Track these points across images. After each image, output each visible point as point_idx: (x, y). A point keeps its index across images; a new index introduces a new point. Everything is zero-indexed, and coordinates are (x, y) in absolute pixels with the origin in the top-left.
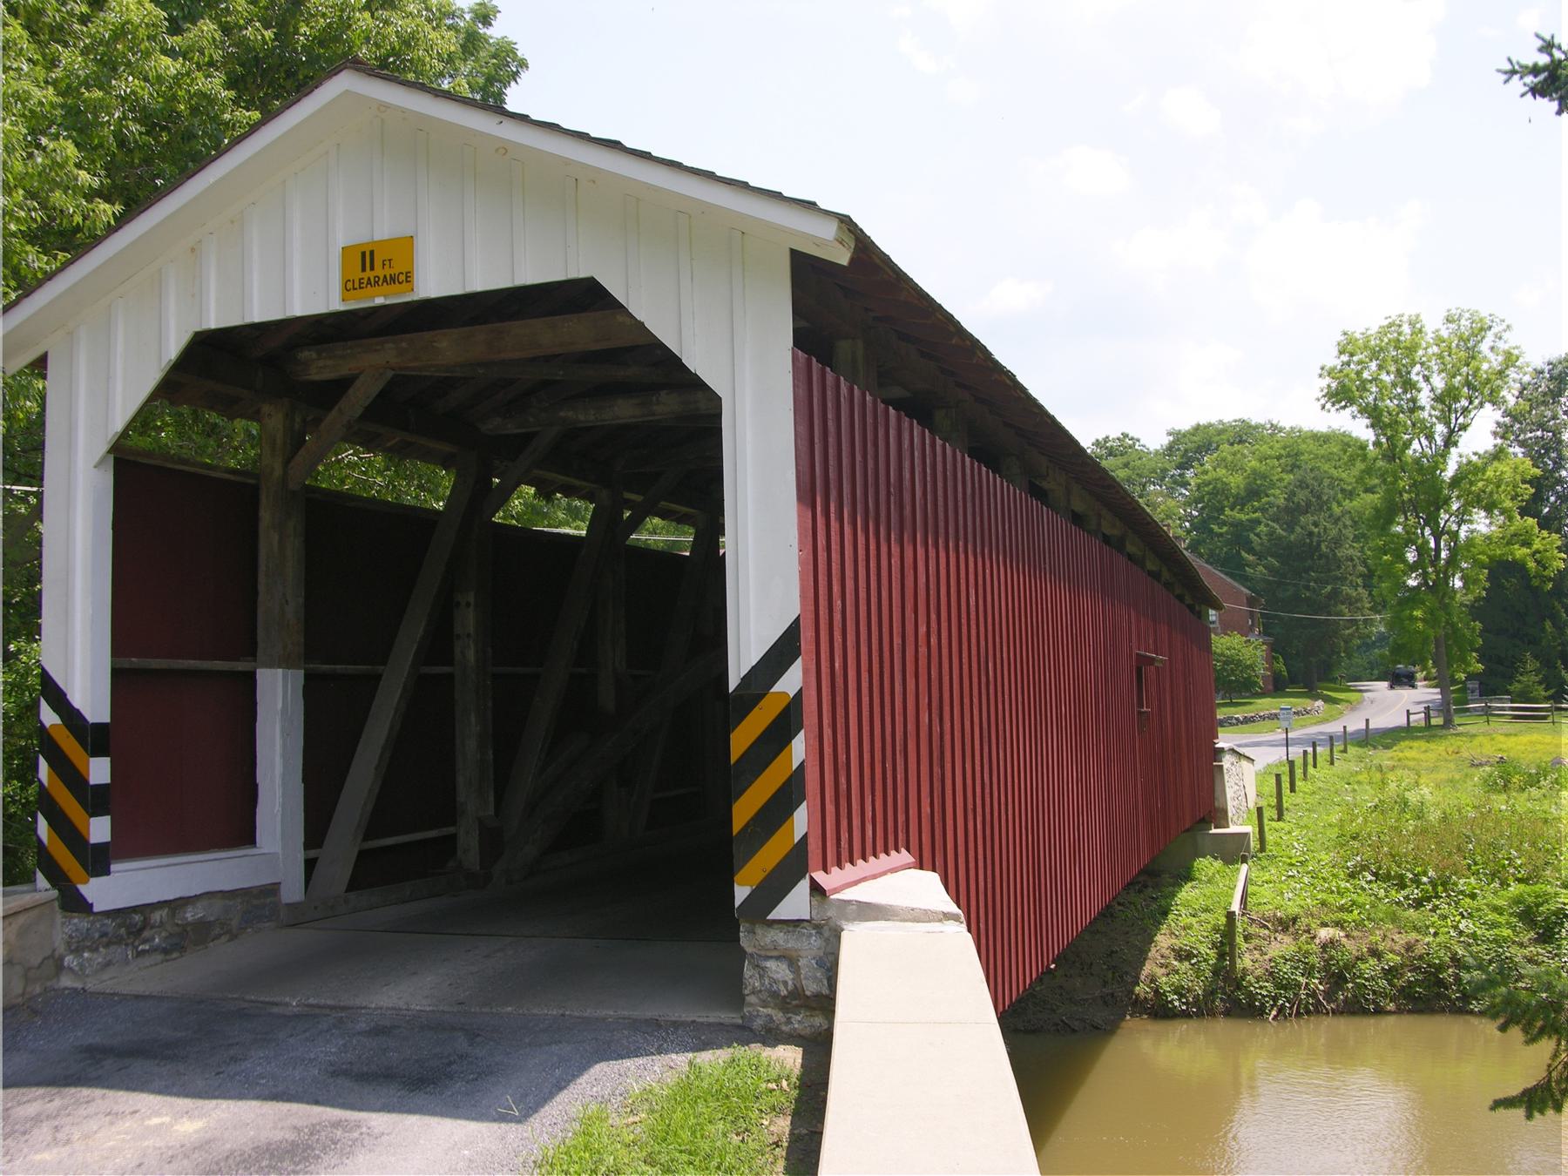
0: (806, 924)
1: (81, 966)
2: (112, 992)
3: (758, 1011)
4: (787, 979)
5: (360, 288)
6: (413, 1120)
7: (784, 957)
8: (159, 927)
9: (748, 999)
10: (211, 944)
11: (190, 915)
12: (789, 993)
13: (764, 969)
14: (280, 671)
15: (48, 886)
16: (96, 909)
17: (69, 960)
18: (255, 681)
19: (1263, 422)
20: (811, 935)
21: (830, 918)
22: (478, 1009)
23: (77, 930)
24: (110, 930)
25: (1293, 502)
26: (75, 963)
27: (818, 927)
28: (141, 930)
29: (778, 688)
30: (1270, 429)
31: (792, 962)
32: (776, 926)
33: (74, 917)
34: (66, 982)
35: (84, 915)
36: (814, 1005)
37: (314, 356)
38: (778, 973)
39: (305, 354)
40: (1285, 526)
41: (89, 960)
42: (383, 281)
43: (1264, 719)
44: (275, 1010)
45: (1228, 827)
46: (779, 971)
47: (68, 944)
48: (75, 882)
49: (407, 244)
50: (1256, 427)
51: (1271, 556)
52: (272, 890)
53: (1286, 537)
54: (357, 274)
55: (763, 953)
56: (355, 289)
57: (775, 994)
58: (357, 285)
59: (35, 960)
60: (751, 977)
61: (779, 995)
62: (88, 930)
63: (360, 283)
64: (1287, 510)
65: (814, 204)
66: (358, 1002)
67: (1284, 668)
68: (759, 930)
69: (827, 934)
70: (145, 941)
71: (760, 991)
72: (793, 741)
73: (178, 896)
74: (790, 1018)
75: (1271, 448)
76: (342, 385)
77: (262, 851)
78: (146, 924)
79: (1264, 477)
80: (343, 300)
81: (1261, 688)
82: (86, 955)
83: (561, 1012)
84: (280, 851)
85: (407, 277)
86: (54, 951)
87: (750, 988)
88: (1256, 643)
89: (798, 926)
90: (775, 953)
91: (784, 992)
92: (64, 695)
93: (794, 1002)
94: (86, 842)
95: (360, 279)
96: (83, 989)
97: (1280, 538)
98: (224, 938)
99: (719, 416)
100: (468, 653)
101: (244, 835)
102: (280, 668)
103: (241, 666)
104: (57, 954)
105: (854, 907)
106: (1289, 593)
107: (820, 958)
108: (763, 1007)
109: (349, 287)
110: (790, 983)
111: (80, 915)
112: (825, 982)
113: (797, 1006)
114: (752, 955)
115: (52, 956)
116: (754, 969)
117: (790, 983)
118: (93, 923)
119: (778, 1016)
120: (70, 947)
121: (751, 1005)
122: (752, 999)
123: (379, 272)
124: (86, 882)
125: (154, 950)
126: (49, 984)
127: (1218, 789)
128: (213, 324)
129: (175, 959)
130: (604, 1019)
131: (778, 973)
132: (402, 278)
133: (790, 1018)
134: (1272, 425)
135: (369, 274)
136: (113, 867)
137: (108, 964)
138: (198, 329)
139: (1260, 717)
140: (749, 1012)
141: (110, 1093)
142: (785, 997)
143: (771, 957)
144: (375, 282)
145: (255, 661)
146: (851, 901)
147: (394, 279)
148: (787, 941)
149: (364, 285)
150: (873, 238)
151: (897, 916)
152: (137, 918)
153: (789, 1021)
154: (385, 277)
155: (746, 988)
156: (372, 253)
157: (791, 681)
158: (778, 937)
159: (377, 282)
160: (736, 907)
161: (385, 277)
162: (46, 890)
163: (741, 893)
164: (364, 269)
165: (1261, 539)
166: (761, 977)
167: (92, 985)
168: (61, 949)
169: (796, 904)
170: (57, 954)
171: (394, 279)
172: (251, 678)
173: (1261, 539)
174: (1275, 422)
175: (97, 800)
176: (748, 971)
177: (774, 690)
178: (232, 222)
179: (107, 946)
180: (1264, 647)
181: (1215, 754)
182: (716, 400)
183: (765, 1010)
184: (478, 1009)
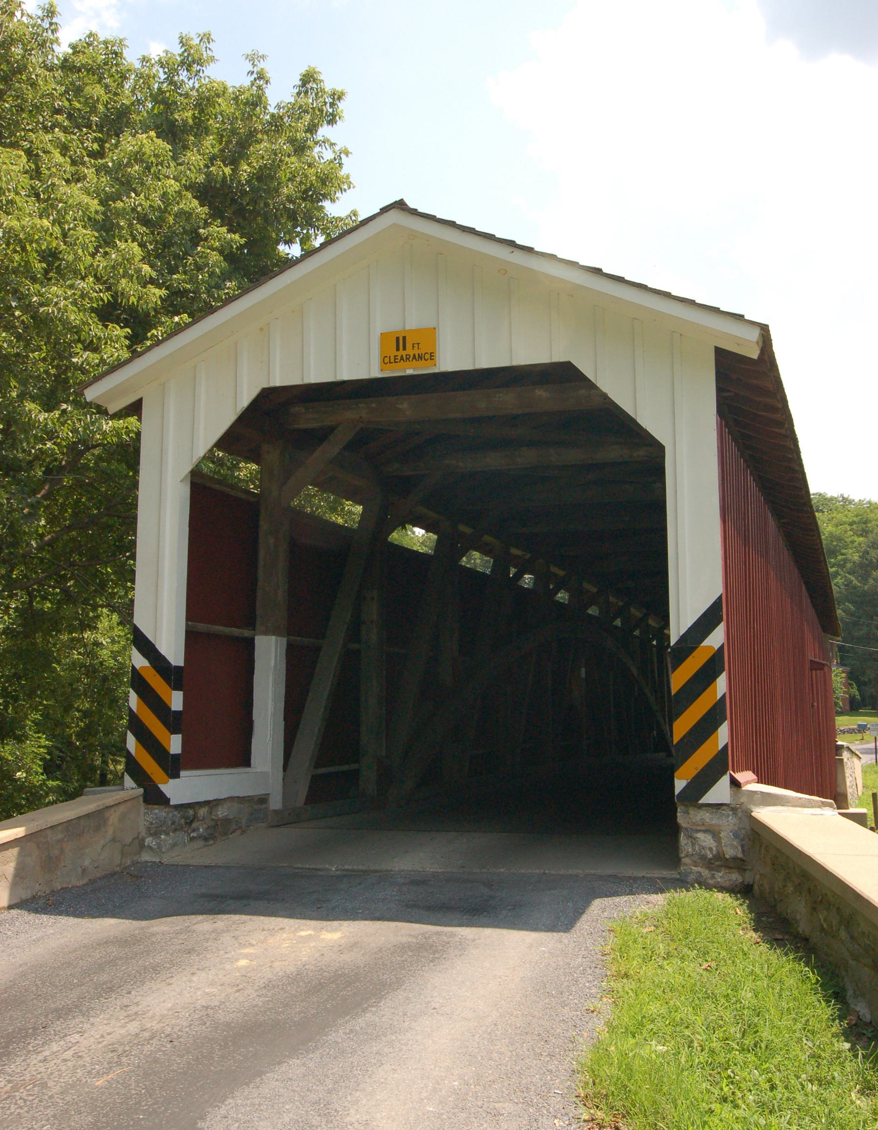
0: (725, 807)
1: (159, 846)
2: (184, 864)
3: (691, 869)
4: (711, 846)
5: (395, 362)
6: (488, 931)
7: (709, 831)
8: (201, 820)
9: (683, 860)
10: (231, 836)
11: (221, 812)
12: (714, 856)
13: (695, 839)
14: (274, 637)
15: (134, 785)
16: (172, 803)
17: (148, 841)
18: (254, 644)
19: (836, 496)
20: (728, 816)
21: (742, 803)
22: (478, 870)
23: (157, 818)
24: (177, 820)
25: (867, 559)
26: (154, 843)
27: (734, 810)
28: (192, 821)
29: (706, 643)
30: (842, 500)
31: (715, 834)
32: (704, 808)
33: (155, 809)
34: (146, 857)
35: (163, 807)
36: (731, 865)
37: (303, 410)
38: (705, 842)
39: (296, 409)
40: (860, 578)
41: (165, 840)
42: (413, 359)
43: (844, 733)
44: (321, 873)
45: (848, 809)
46: (706, 840)
47: (149, 829)
48: (157, 782)
49: (431, 333)
50: (832, 499)
51: (850, 602)
52: (263, 800)
53: (861, 587)
54: (393, 352)
55: (694, 828)
56: (390, 363)
57: (703, 857)
58: (392, 360)
59: (128, 840)
60: (686, 845)
61: (706, 858)
62: (165, 818)
63: (395, 359)
64: (861, 565)
65: (743, 316)
66: (384, 867)
67: (857, 693)
68: (692, 811)
69: (740, 814)
70: (194, 831)
71: (692, 855)
72: (717, 680)
73: (215, 798)
74: (714, 874)
75: (846, 516)
76: (331, 429)
77: (255, 770)
78: (195, 817)
79: (839, 539)
80: (382, 370)
81: (840, 708)
82: (163, 837)
83: (542, 871)
84: (270, 771)
85: (431, 356)
86: (139, 833)
87: (685, 852)
88: (837, 671)
89: (719, 809)
90: (703, 828)
91: (710, 856)
92: (154, 646)
93: (717, 863)
94: (167, 753)
95: (395, 356)
96: (160, 862)
97: (855, 587)
98: (238, 833)
99: (663, 457)
100: (372, 635)
101: (243, 759)
102: (273, 634)
103: (246, 633)
104: (140, 836)
105: (759, 796)
106: (862, 632)
107: (736, 831)
108: (695, 866)
109: (385, 361)
110: (714, 849)
111: (160, 807)
112: (740, 848)
113: (718, 866)
114: (686, 829)
115: (137, 838)
116: (688, 839)
117: (714, 849)
118: (168, 813)
119: (705, 873)
120: (149, 831)
121: (686, 865)
122: (686, 860)
123: (409, 351)
124: (166, 782)
125: (199, 837)
126: (135, 858)
127: (839, 778)
128: (278, 382)
129: (211, 845)
130: (577, 876)
131: (705, 842)
132: (427, 356)
133: (714, 874)
134: (843, 498)
135: (401, 352)
136: (182, 773)
137: (174, 845)
138: (266, 386)
139: (841, 731)
140: (684, 869)
141: (255, 918)
142: (711, 859)
143: (700, 831)
144: (407, 359)
145: (254, 630)
146: (756, 792)
147: (420, 357)
148: (711, 819)
149: (398, 360)
150: (774, 342)
151: (789, 802)
152: (191, 812)
153: (713, 877)
154: (414, 355)
155: (682, 853)
156: (404, 338)
157: (716, 638)
158: (705, 816)
159: (408, 359)
160: (676, 794)
161: (414, 355)
162: (132, 789)
163: (680, 785)
164: (398, 349)
165: (840, 588)
166: (693, 844)
167: (166, 860)
168: (143, 833)
169: (719, 792)
170: (140, 836)
171: (420, 357)
172: (250, 644)
173: (840, 588)
174: (846, 496)
175: (173, 721)
176: (683, 840)
177: (702, 644)
178: (293, 311)
179: (175, 830)
180: (844, 675)
181: (837, 750)
182: (661, 448)
183: (696, 869)
184: (478, 870)
